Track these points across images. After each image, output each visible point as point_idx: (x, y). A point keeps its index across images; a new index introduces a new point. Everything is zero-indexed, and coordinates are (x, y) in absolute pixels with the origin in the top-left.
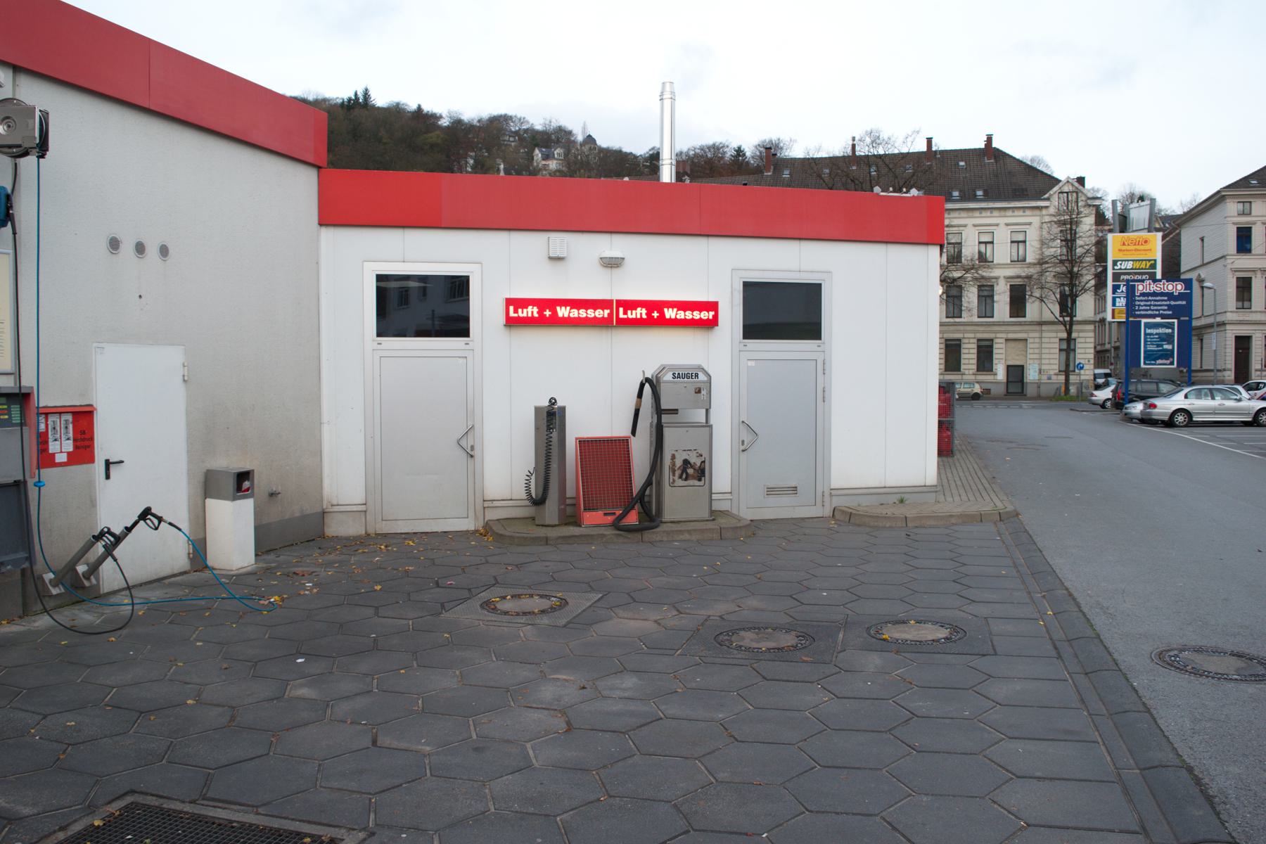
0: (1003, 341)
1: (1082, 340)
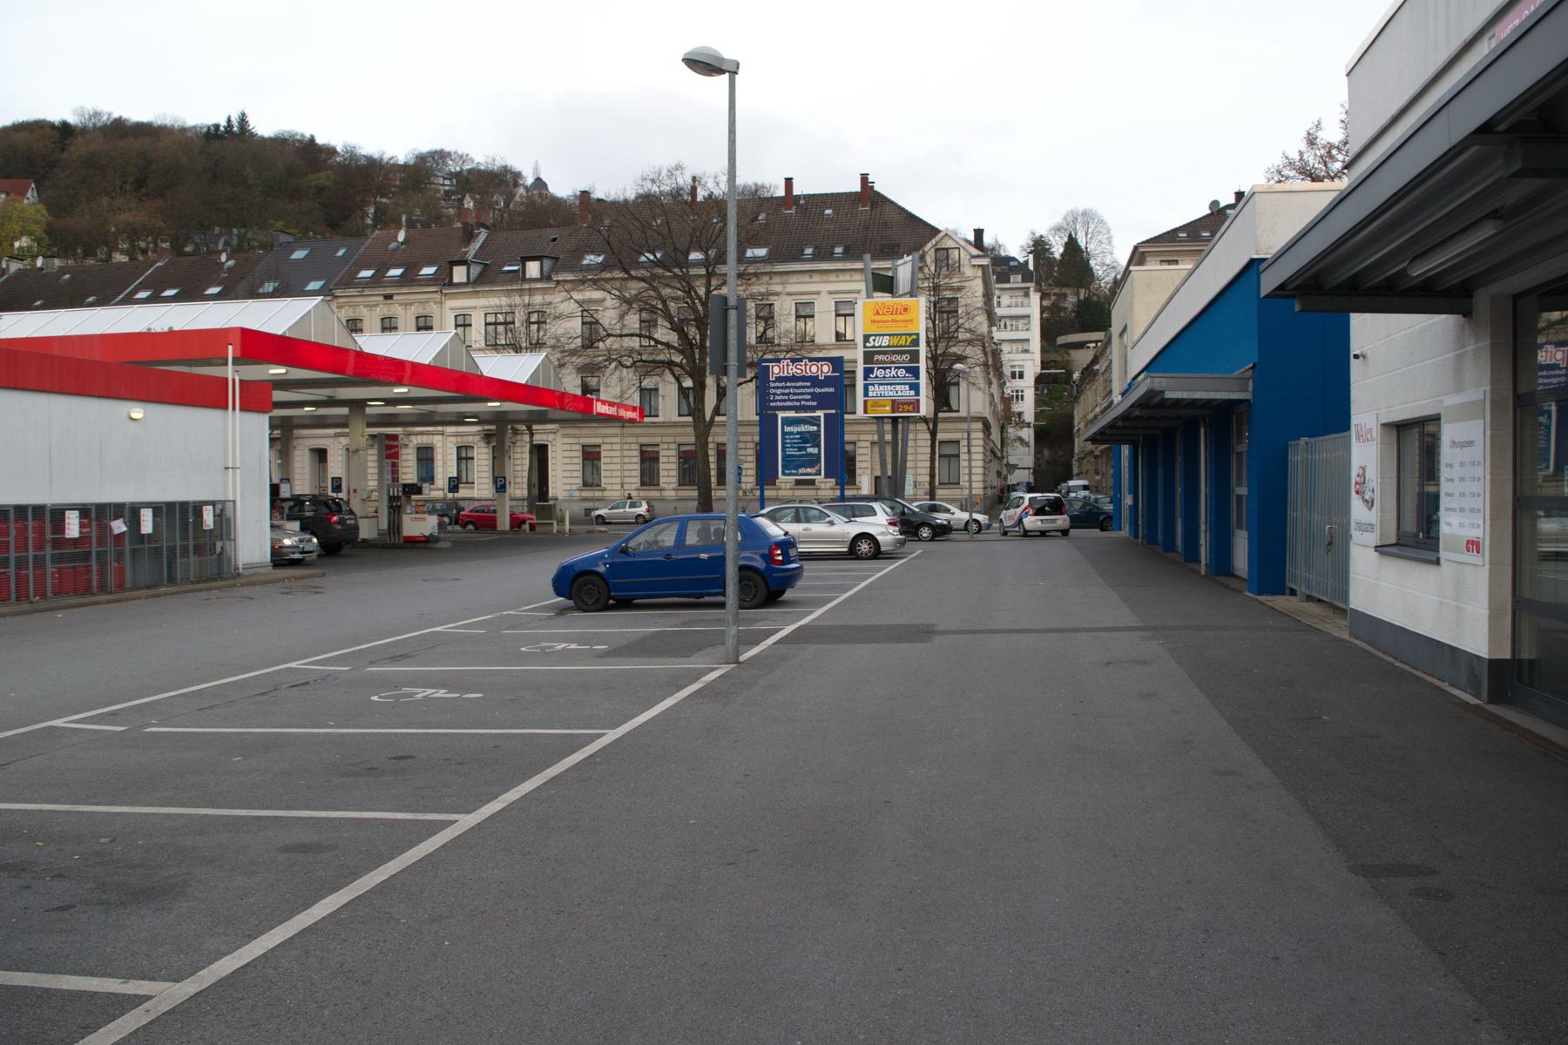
0: (868, 444)
1: (609, 447)
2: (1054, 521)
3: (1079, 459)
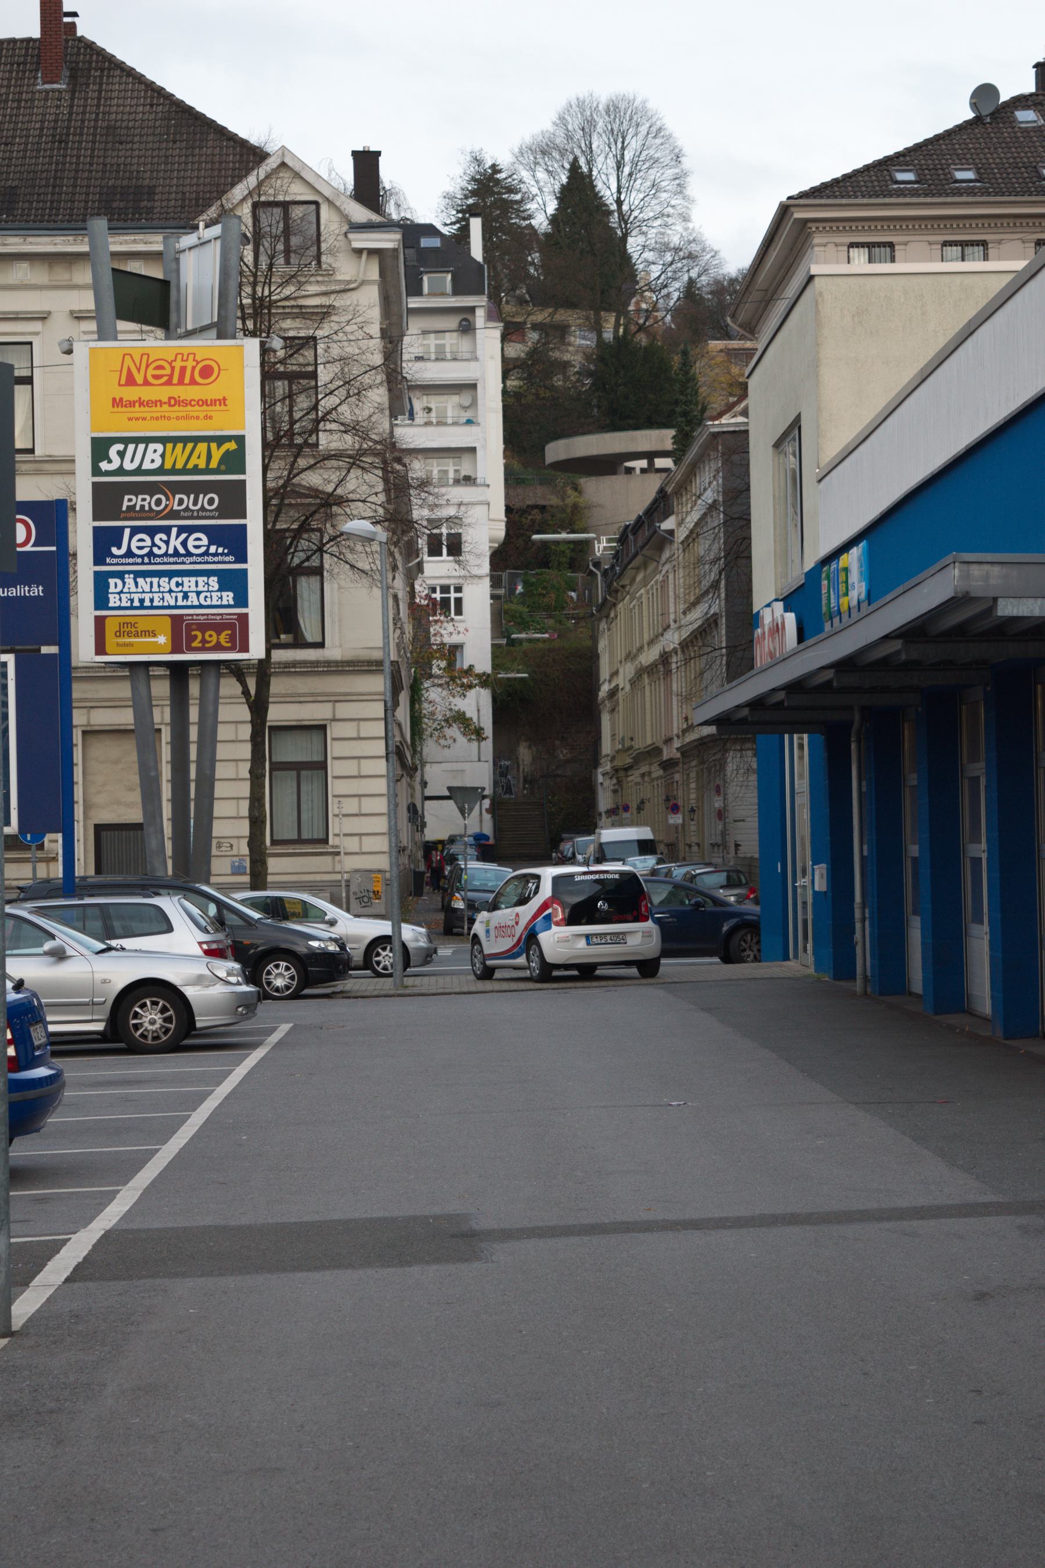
2: (619, 938)
3: (616, 770)
